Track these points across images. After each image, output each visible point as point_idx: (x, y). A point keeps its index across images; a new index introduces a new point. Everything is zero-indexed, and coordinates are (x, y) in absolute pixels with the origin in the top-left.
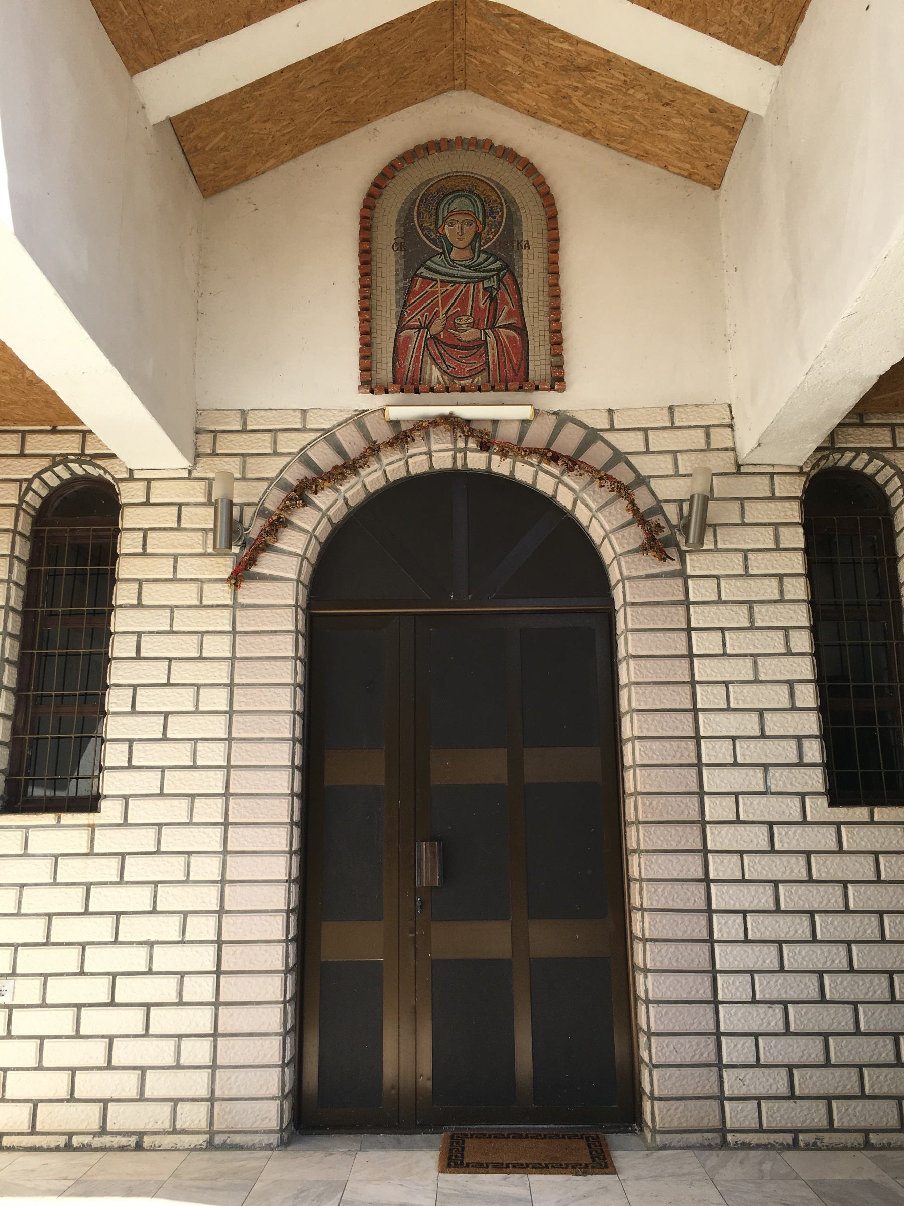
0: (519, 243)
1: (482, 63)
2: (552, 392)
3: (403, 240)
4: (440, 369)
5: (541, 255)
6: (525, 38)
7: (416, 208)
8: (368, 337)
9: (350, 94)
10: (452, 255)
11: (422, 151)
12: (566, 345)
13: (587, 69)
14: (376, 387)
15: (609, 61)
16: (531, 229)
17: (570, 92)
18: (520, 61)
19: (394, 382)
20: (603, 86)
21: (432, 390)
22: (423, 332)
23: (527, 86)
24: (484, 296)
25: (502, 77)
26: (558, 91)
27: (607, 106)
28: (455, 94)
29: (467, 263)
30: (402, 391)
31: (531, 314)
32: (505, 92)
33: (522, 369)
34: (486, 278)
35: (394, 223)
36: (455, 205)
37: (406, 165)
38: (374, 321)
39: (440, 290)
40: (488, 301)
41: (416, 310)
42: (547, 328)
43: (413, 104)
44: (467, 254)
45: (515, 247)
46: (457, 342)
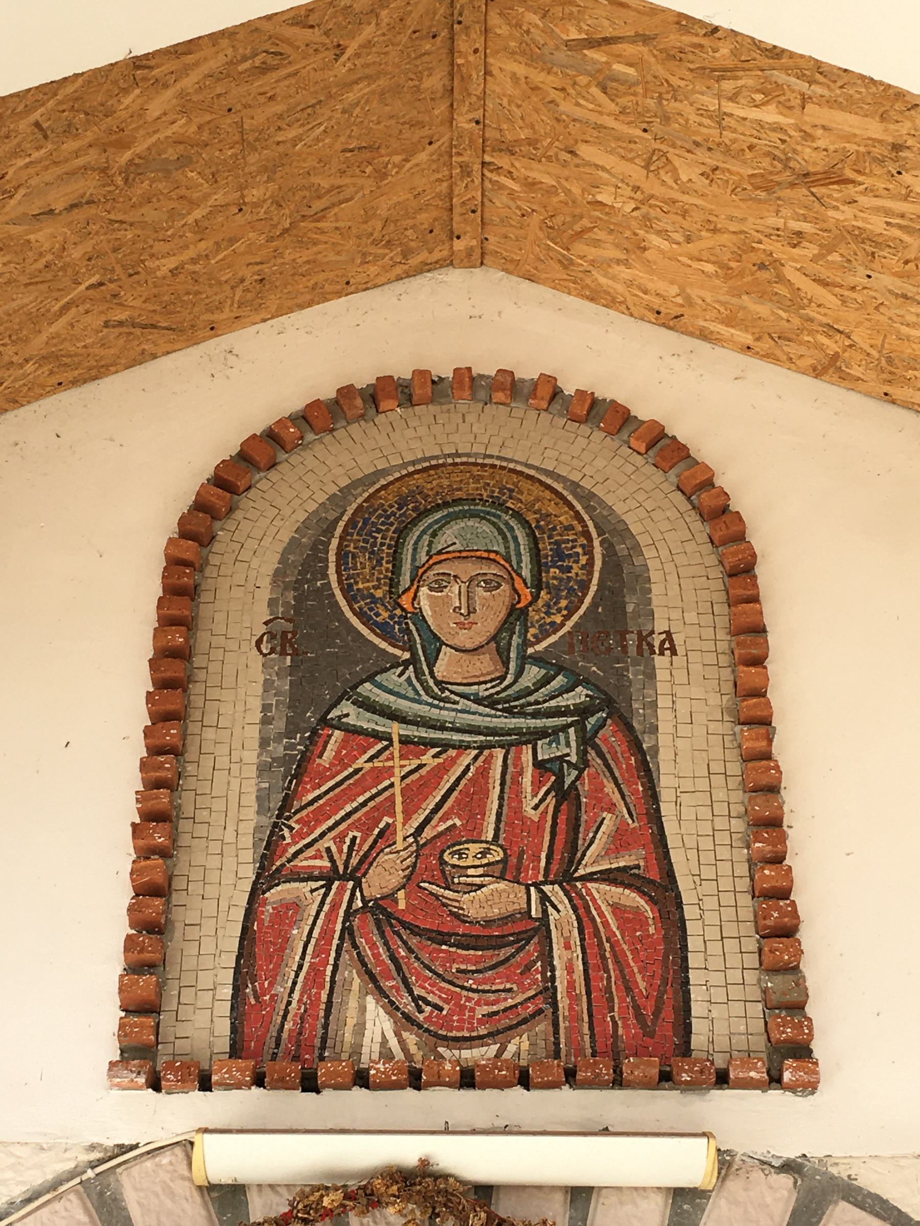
0: (641, 638)
1: (531, 185)
2: (775, 1095)
3: (289, 626)
4: (392, 1008)
5: (712, 672)
6: (651, 103)
7: (335, 543)
8: (157, 902)
9: (159, 247)
10: (441, 669)
11: (359, 402)
12: (807, 936)
13: (832, 177)
14: (170, 1065)
15: (897, 147)
16: (679, 594)
17: (779, 250)
18: (636, 173)
19: (236, 1051)
20: (876, 224)
21: (362, 1079)
22: (341, 890)
23: (655, 240)
24: (537, 784)
25: (585, 222)
26: (745, 248)
27: (886, 281)
28: (454, 277)
29: (483, 691)
30: (259, 1081)
31: (690, 842)
32: (592, 263)
33: (668, 1014)
34: (543, 733)
35: (266, 582)
36: (449, 536)
37: (310, 437)
38: (182, 857)
39: (400, 766)
40: (551, 801)
41: (319, 822)
42: (744, 884)
43: (339, 294)
44: (485, 665)
45: (632, 650)
46: (449, 925)
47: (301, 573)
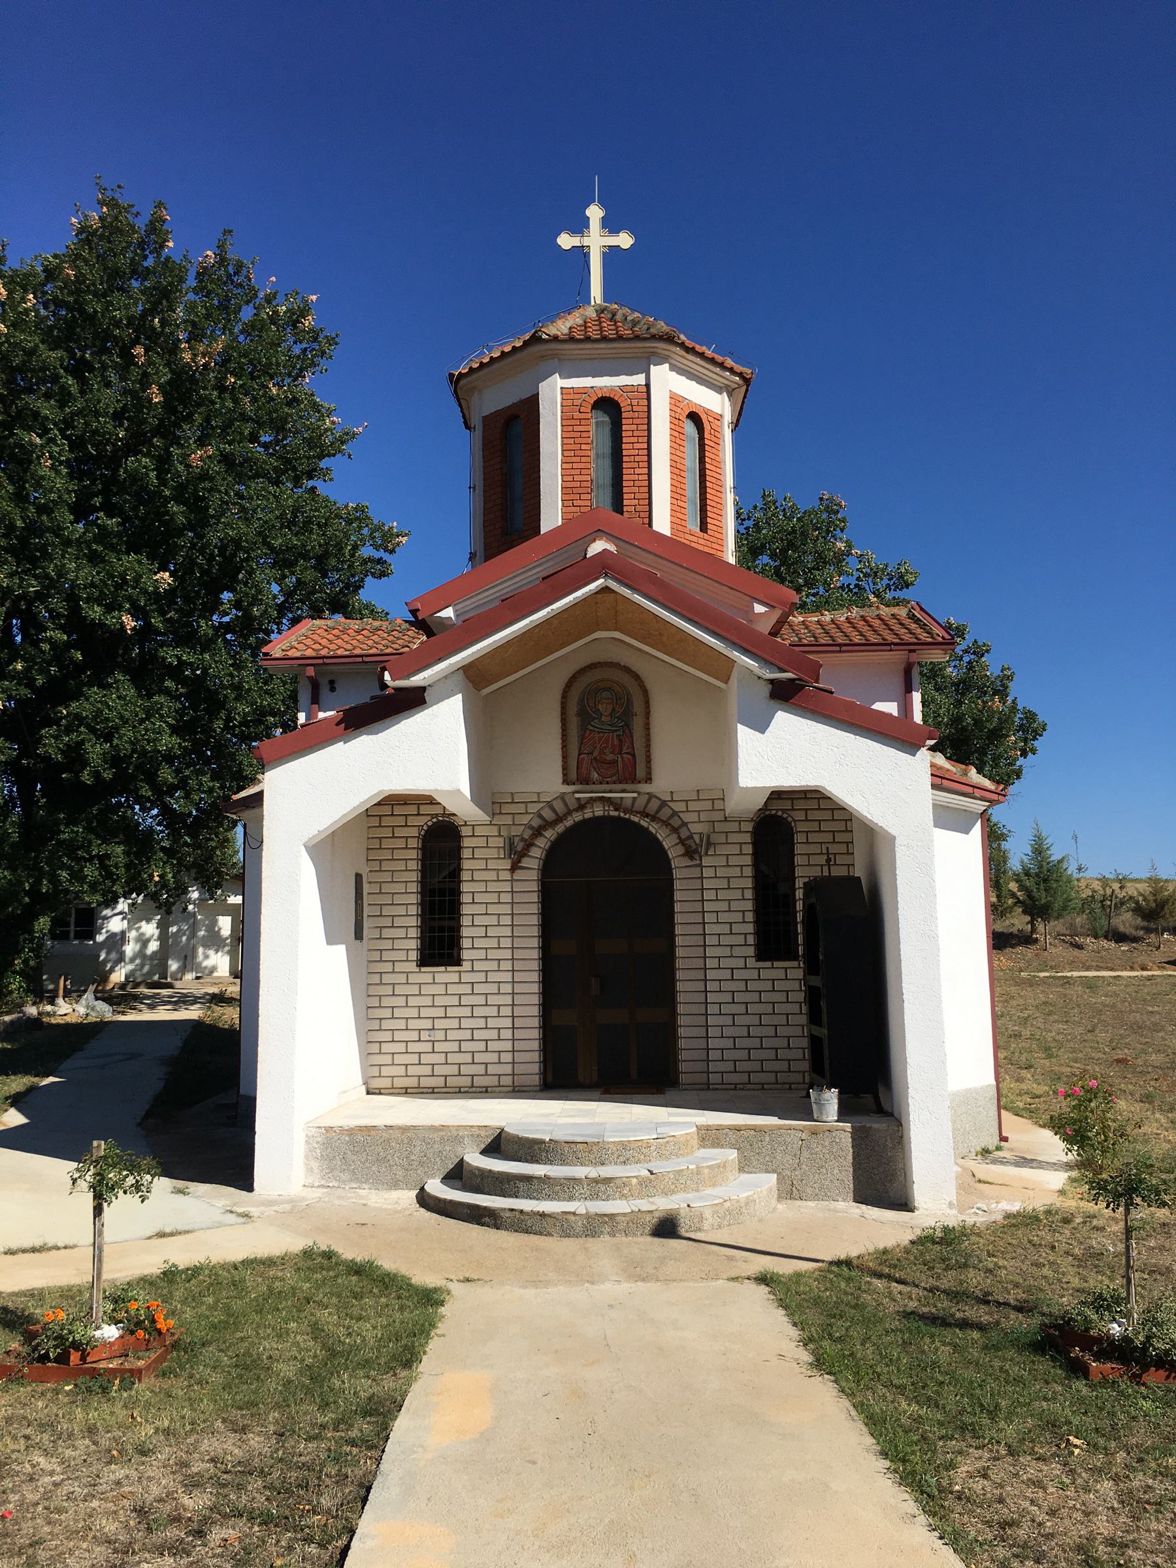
16: (638, 707)
47: (581, 702)
